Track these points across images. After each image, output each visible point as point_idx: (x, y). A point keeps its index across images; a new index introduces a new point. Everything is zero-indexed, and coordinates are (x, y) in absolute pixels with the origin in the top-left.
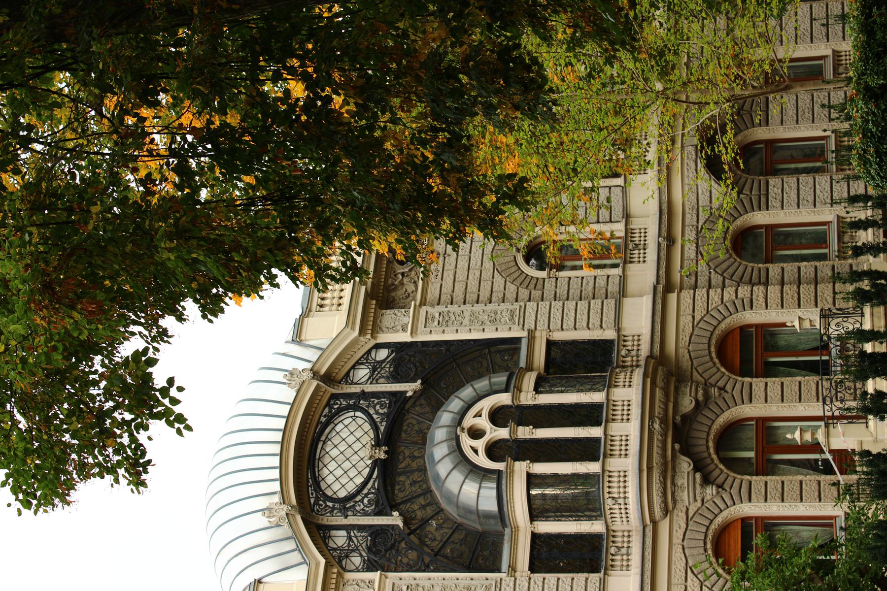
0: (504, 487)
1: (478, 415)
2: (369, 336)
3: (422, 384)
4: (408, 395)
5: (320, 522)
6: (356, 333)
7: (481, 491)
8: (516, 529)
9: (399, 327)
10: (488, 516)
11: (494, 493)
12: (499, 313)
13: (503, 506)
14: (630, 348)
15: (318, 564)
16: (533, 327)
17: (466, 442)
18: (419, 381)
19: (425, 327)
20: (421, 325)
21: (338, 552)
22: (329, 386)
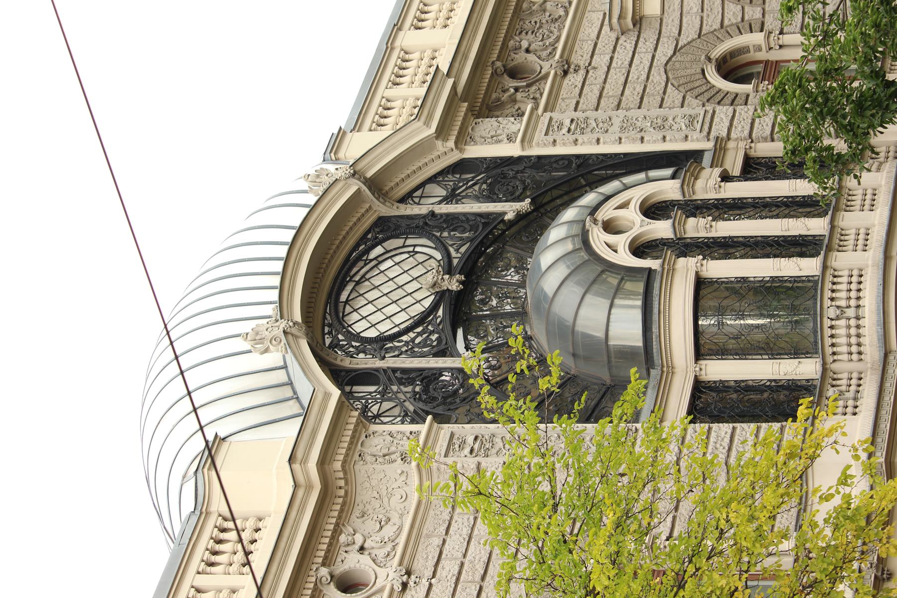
0: (656, 292)
1: (624, 206)
2: (451, 144)
3: (531, 203)
4: (506, 218)
5: (338, 362)
6: (433, 129)
7: (613, 311)
8: (669, 371)
9: (504, 136)
10: (627, 355)
11: (638, 315)
12: (670, 119)
13: (652, 323)
14: (844, 388)
15: (327, 396)
16: (724, 134)
17: (599, 239)
18: (528, 200)
19: (546, 134)
20: (539, 135)
21: (363, 401)
22: (378, 199)
